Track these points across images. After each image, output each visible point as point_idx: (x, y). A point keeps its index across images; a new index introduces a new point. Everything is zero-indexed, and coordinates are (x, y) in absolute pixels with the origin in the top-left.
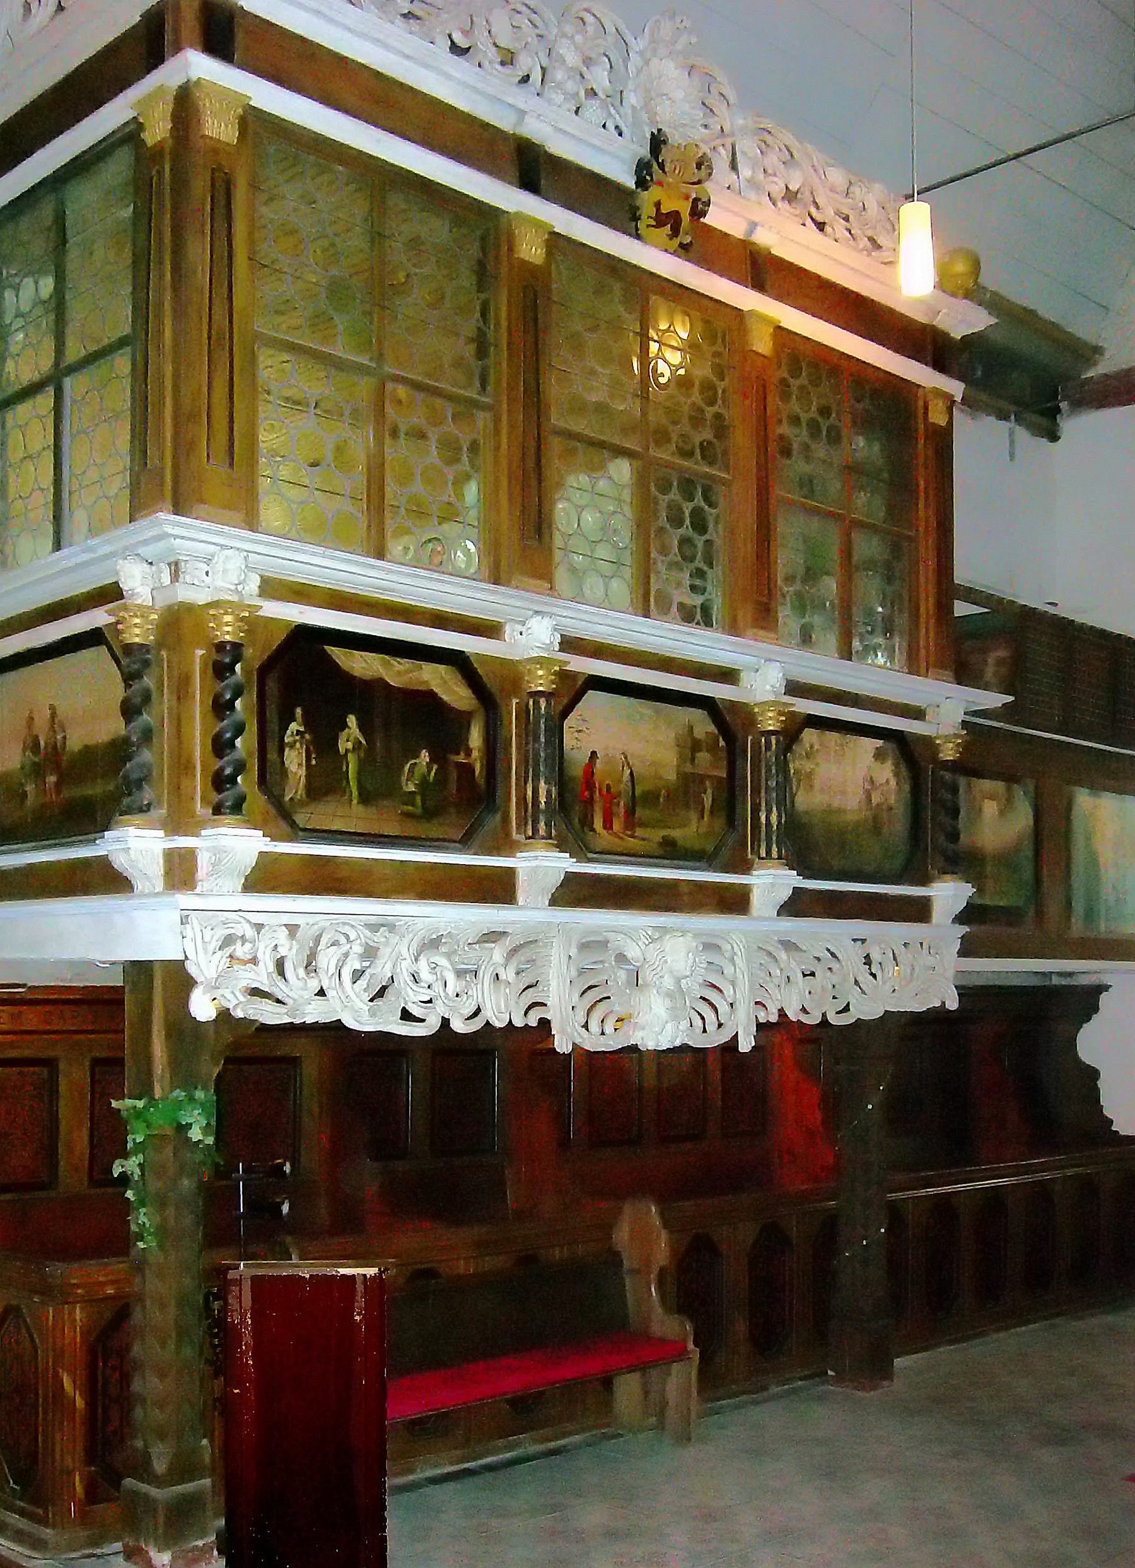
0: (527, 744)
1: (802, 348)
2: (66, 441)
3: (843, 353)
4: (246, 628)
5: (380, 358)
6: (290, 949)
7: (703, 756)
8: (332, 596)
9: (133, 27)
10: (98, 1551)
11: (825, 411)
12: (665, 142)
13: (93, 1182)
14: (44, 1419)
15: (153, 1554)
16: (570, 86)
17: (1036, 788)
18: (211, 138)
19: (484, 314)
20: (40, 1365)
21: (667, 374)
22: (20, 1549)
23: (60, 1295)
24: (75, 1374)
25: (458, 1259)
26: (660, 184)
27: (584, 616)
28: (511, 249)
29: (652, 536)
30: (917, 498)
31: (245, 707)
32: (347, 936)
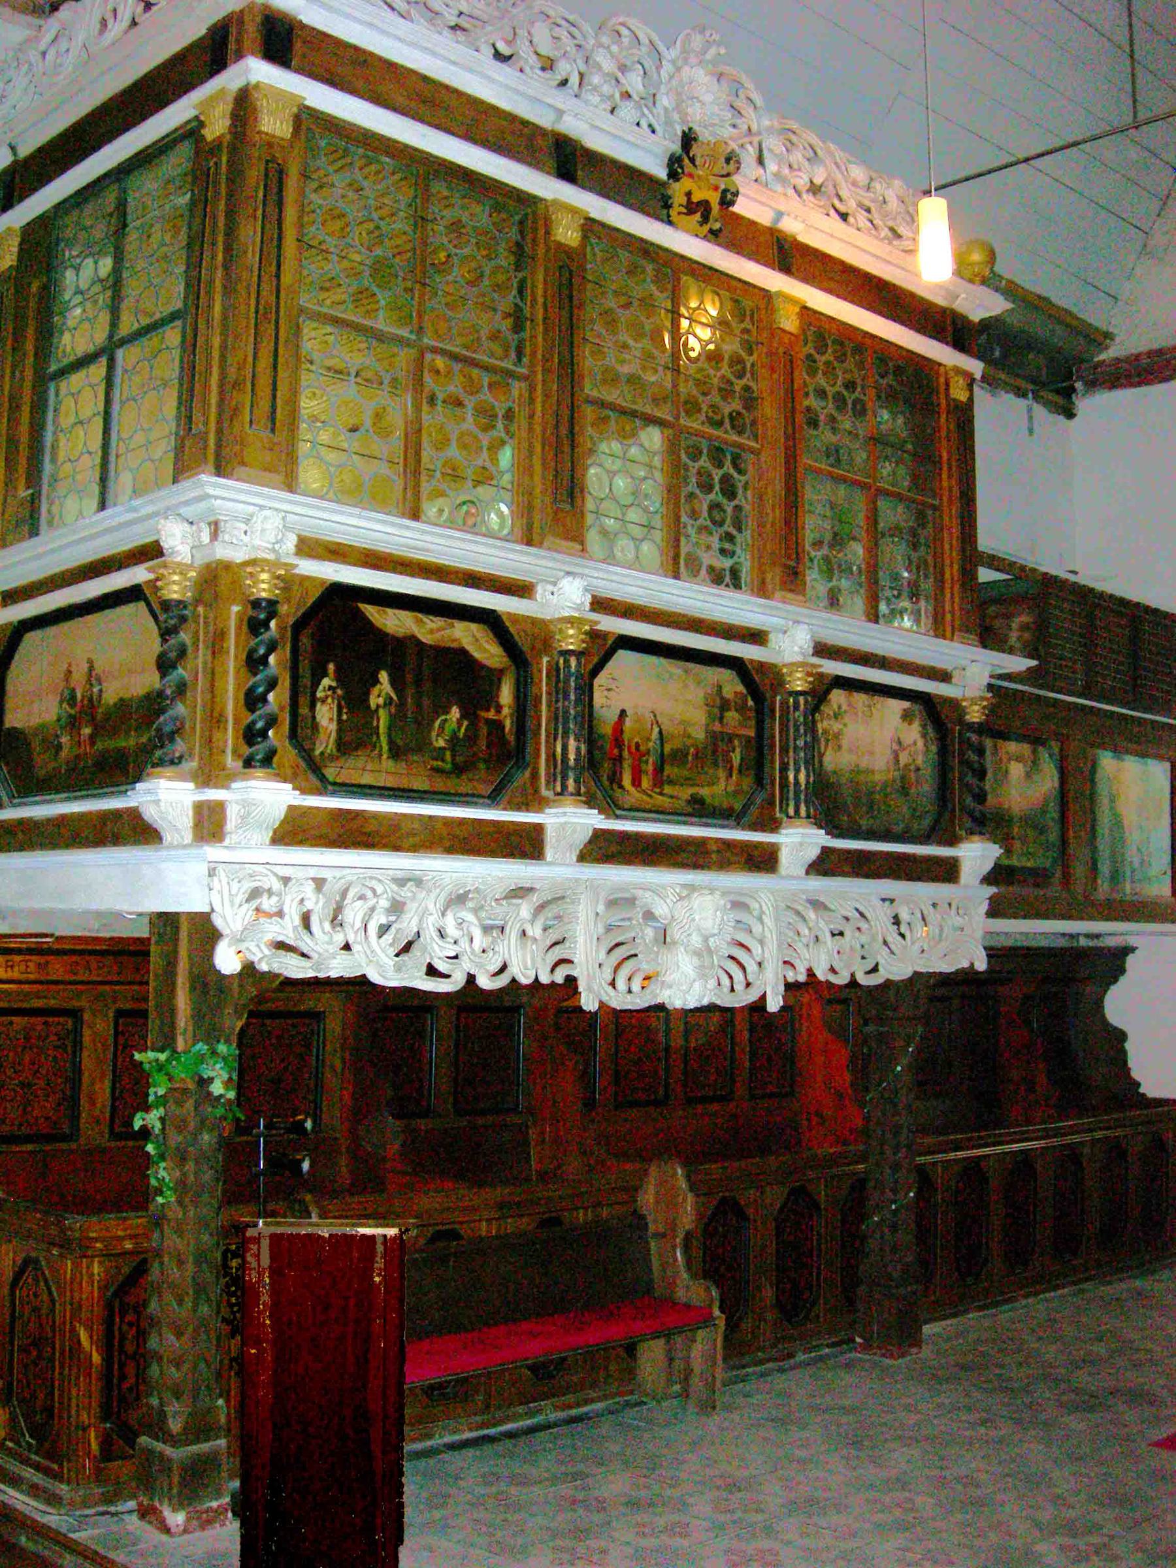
0: (557, 701)
1: (827, 326)
2: (116, 408)
3: (867, 333)
4: (282, 585)
5: (420, 330)
6: (317, 903)
7: (732, 716)
8: (367, 556)
9: (200, 39)
10: (112, 1509)
11: (850, 386)
12: (695, 139)
13: (114, 1135)
14: (61, 1374)
15: (166, 1512)
16: (606, 89)
17: (1061, 750)
18: (267, 134)
19: (521, 292)
20: (57, 1318)
21: (698, 348)
22: (35, 1504)
23: (81, 1248)
24: (92, 1328)
25: (480, 1220)
26: (691, 175)
27: (614, 578)
28: (548, 233)
29: (683, 501)
30: (941, 469)
31: (279, 663)
32: (374, 891)
